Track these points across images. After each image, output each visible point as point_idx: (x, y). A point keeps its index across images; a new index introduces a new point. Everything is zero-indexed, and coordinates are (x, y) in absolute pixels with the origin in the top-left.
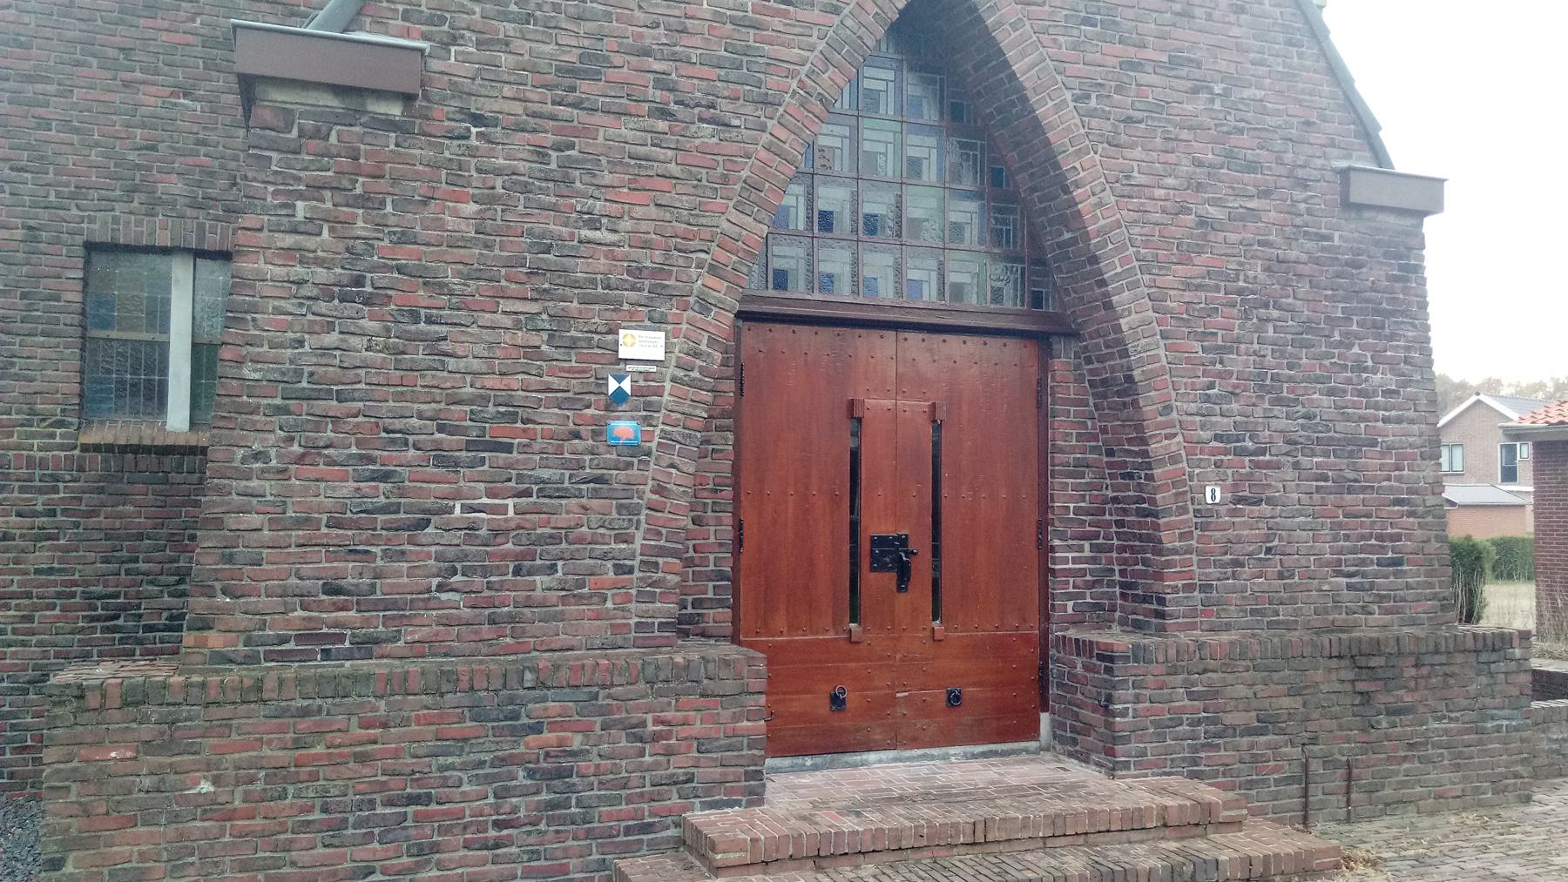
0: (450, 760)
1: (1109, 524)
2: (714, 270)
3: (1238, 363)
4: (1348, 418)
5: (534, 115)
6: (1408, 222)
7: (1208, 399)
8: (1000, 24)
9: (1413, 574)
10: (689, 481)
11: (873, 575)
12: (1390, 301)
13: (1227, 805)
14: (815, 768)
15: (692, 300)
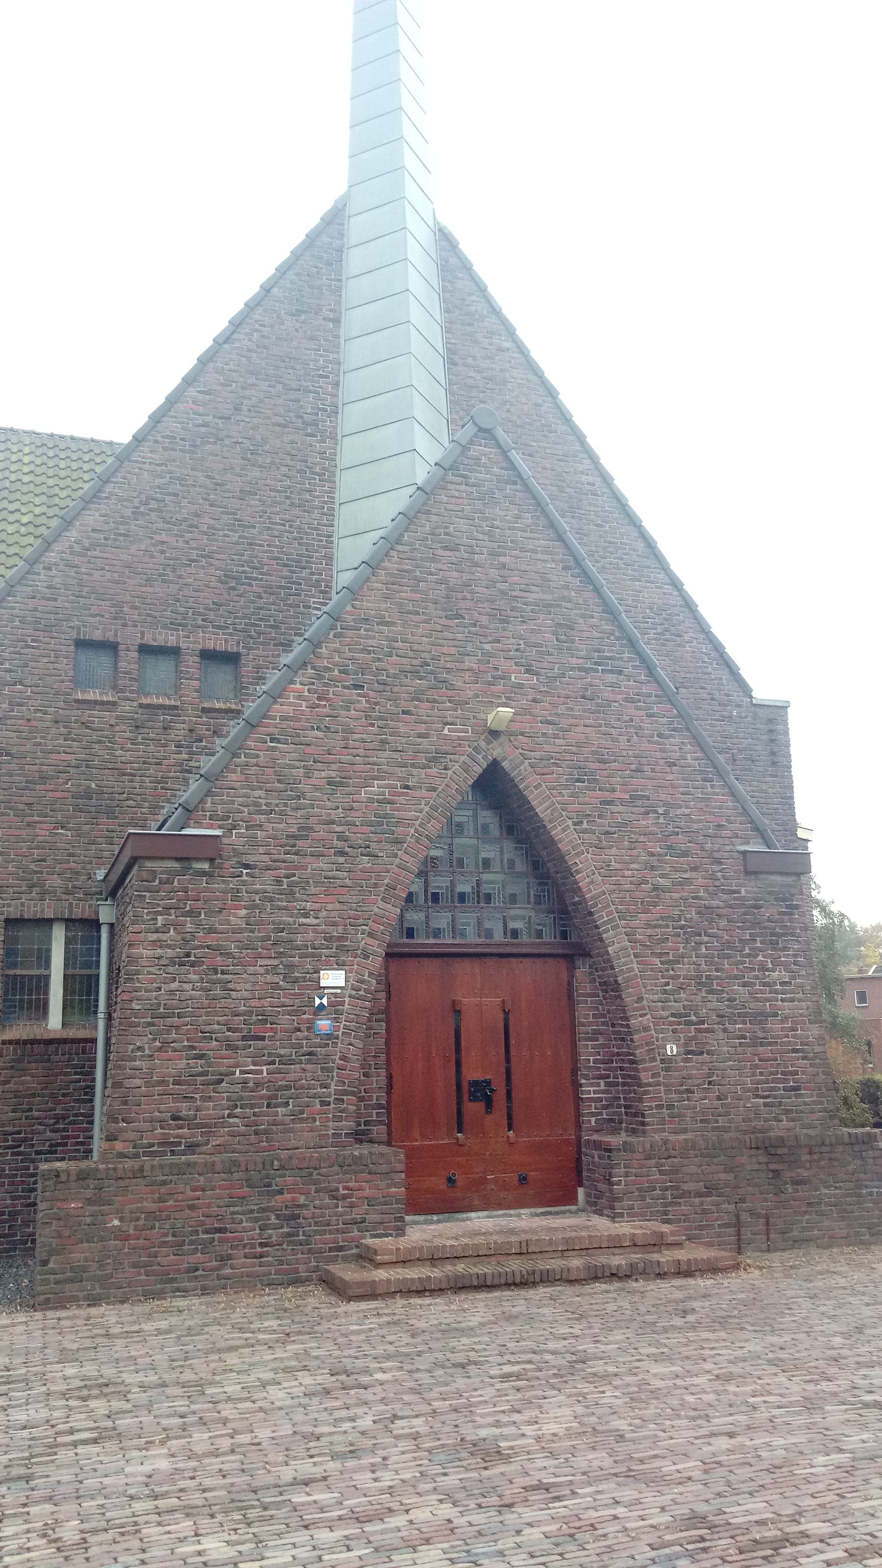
0: (236, 1209)
1: (616, 1069)
2: (370, 935)
3: (683, 969)
4: (758, 1000)
5: (275, 861)
6: (790, 880)
7: (665, 992)
8: (527, 787)
9: (808, 1097)
10: (360, 1052)
11: (470, 1104)
12: (781, 927)
13: (673, 1233)
14: (439, 1221)
15: (359, 952)
